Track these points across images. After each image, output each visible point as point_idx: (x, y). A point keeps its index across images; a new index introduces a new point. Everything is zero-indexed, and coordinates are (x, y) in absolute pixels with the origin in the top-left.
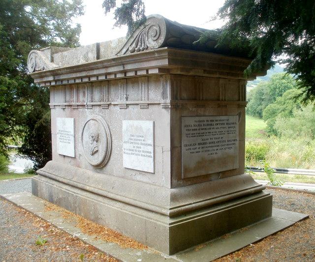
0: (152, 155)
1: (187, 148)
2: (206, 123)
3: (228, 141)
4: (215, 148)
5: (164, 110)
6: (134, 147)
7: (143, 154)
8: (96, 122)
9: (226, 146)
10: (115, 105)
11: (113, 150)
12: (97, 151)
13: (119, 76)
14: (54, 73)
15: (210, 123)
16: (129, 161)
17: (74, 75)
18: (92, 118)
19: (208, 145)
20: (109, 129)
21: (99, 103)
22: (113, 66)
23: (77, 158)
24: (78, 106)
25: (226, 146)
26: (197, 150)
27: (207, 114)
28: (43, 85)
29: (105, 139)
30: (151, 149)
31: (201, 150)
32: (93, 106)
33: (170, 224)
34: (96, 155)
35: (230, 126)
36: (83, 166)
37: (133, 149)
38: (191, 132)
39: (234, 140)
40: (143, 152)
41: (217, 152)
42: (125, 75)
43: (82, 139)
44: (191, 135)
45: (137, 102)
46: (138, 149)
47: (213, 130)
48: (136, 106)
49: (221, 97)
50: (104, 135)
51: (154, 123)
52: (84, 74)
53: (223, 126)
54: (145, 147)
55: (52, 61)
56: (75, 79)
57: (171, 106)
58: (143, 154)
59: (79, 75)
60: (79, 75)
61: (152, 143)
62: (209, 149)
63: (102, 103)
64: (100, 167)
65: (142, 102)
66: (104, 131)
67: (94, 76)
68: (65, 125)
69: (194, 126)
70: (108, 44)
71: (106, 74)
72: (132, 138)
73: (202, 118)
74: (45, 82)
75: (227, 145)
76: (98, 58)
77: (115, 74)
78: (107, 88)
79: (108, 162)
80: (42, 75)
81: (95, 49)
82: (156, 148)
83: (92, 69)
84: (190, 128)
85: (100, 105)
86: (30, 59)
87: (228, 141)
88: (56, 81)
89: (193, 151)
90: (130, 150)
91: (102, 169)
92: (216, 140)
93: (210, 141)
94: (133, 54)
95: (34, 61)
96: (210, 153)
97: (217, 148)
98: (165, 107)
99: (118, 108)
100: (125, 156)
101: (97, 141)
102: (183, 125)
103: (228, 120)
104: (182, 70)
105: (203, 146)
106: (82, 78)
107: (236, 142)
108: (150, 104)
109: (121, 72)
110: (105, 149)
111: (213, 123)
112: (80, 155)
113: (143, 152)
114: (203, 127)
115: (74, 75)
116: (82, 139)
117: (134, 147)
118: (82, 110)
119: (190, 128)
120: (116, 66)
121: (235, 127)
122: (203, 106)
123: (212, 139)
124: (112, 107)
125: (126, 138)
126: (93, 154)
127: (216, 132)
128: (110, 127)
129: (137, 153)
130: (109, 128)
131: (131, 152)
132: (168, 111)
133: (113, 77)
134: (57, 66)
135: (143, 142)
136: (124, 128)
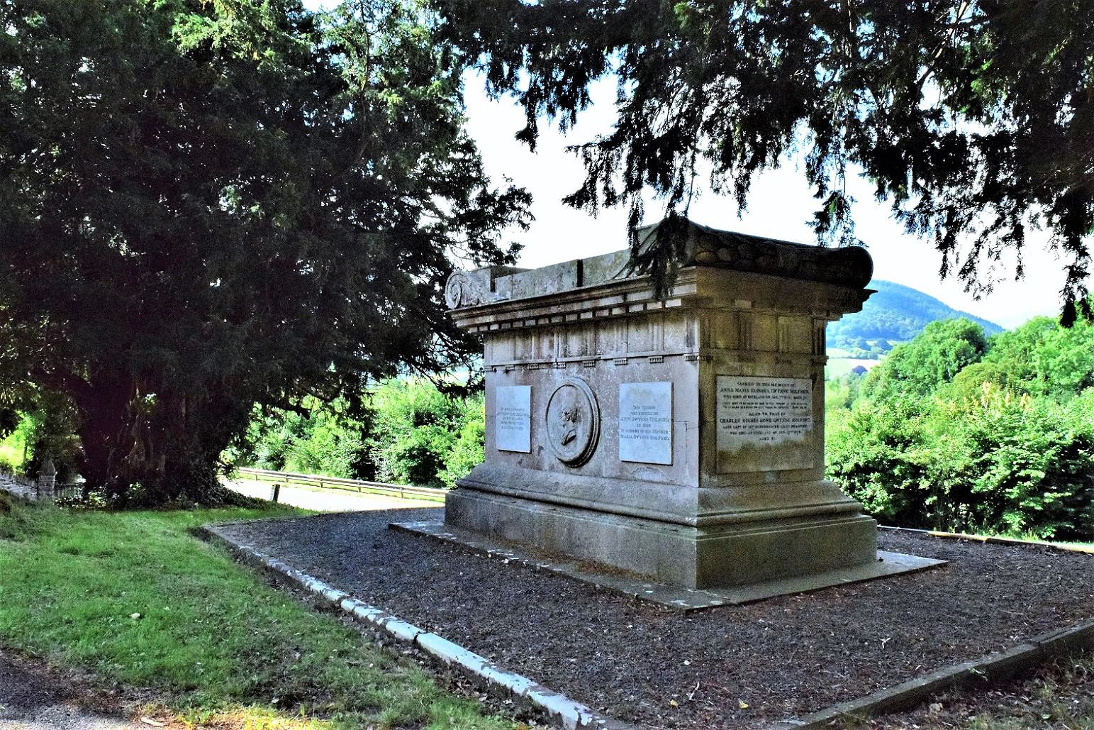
0: (669, 435)
1: (726, 424)
2: (755, 387)
3: (793, 420)
4: (772, 430)
5: (689, 363)
6: (639, 426)
7: (654, 435)
8: (574, 390)
9: (790, 429)
10: (605, 360)
11: (602, 433)
12: (573, 438)
13: (616, 312)
14: (496, 309)
15: (761, 388)
16: (627, 450)
17: (536, 312)
18: (566, 383)
19: (759, 424)
20: (596, 400)
21: (578, 359)
22: (607, 297)
23: (535, 453)
24: (539, 364)
25: (790, 429)
26: (741, 430)
27: (758, 374)
28: (475, 330)
29: (589, 416)
30: (667, 426)
31: (747, 430)
32: (566, 363)
33: (697, 538)
34: (571, 444)
35: (796, 395)
36: (546, 467)
37: (637, 428)
38: (732, 400)
39: (805, 420)
40: (655, 431)
41: (775, 436)
42: (627, 310)
43: (546, 420)
44: (731, 405)
45: (645, 354)
46: (646, 428)
47: (768, 400)
48: (642, 360)
49: (781, 347)
50: (587, 410)
51: (673, 385)
52: (554, 310)
53: (785, 394)
54: (658, 423)
55: (493, 289)
56: (537, 318)
57: (701, 356)
58: (654, 435)
59: (544, 312)
60: (544, 312)
61: (670, 417)
62: (763, 430)
63: (584, 358)
64: (578, 463)
65: (653, 353)
66: (587, 403)
67: (572, 312)
68: (513, 398)
69: (737, 390)
70: (596, 261)
71: (594, 310)
72: (636, 411)
73: (748, 380)
74: (478, 326)
75: (793, 426)
76: (580, 283)
77: (610, 308)
78: (593, 332)
79: (592, 454)
80: (475, 311)
81: (574, 269)
82: (675, 425)
83: (549, 305)
84: (729, 394)
85: (581, 361)
86: (450, 286)
87: (793, 420)
88: (500, 323)
89: (735, 430)
90: (632, 431)
91: (580, 467)
92: (773, 417)
93: (762, 417)
94: (641, 277)
95: (459, 290)
96: (762, 436)
97: (776, 430)
98: (692, 359)
99: (611, 364)
100: (623, 443)
101: (574, 421)
102: (719, 389)
103: (793, 385)
104: (647, 393)
105: (750, 424)
106: (550, 316)
107: (808, 423)
108: (666, 356)
109: (619, 306)
110: (588, 433)
111: (767, 388)
112: (541, 448)
113: (655, 431)
114: (750, 394)
115: (536, 312)
116: (546, 420)
117: (639, 426)
118: (546, 371)
119: (729, 394)
120: (612, 295)
121: (805, 397)
122: (753, 360)
123: (766, 414)
124: (601, 364)
125: (625, 411)
126: (566, 443)
127: (772, 404)
128: (598, 397)
129: (645, 434)
130: (595, 397)
131: (632, 434)
132: (695, 365)
133: (606, 313)
134: (503, 298)
135: (654, 416)
136: (622, 394)
